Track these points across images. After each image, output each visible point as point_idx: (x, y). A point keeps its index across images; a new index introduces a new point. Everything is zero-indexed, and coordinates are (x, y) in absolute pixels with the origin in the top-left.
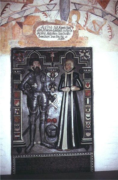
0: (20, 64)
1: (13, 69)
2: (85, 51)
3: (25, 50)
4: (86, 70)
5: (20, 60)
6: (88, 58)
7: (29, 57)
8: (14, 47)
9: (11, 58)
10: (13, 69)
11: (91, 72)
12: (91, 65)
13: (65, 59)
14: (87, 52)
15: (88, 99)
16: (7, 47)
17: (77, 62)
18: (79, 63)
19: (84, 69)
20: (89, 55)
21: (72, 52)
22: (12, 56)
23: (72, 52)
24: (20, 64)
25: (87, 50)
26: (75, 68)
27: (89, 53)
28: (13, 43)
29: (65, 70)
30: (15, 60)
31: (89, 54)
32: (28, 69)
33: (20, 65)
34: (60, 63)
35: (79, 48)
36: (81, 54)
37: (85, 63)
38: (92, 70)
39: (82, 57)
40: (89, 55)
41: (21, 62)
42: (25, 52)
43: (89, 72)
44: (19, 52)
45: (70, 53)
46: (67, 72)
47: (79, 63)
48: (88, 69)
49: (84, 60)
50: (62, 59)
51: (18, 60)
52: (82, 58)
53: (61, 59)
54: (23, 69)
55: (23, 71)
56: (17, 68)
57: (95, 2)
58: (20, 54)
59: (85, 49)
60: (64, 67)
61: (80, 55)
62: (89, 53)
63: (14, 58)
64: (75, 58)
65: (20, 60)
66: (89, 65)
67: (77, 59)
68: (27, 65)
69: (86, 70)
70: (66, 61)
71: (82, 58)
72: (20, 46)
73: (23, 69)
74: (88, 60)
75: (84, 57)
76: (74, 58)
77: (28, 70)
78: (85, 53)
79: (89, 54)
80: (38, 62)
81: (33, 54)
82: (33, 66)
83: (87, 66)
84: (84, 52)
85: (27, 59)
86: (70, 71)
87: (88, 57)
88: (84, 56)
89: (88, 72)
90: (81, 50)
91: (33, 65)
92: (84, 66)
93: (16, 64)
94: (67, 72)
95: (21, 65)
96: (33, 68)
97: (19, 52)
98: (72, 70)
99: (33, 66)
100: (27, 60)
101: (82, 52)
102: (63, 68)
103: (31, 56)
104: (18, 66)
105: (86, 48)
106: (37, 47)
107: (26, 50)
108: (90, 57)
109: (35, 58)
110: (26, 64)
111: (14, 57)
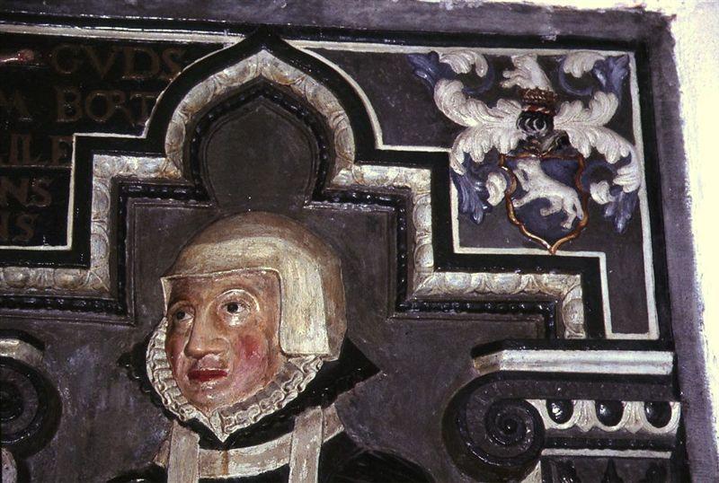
2: (529, 73)
4: (634, 414)
6: (599, 194)
11: (679, 444)
12: (664, 324)
13: (156, 189)
14: (583, 89)
15: (177, 191)
17: (404, 268)
18: (432, 280)
19: (564, 388)
20: (613, 148)
25: (579, 63)
26: (370, 370)
27: (606, 106)
29: (170, 397)
31: (619, 125)
34: (79, 257)
35: (442, 25)
36: (471, 116)
37: (550, 280)
38: (698, 406)
39: (494, 162)
40: (613, 148)
43: (642, 441)
45: (261, 88)
46: (208, 440)
47: (432, 280)
48: (610, 390)
49: (538, 219)
50: (122, 188)
52: (497, 188)
53: (100, 187)
57: (337, 117)
59: (530, 41)
60: (156, 353)
61: (451, 131)
62: (606, 106)
64: (358, 194)
66: (631, 316)
67: (400, 199)
69: (584, 414)
70: (204, 226)
71: (497, 188)
74: (596, 226)
75: (531, 168)
76: (345, 195)
78: (538, 111)
79: (619, 125)
83: (595, 340)
84: (516, 94)
86: (253, 415)
87: (599, 168)
88: (523, 148)
89: (623, 441)
90: (462, 59)
92: (533, 324)
94: (208, 440)
98: (316, 394)
101: (486, 90)
102: (136, 359)
105: (562, 15)
108: (632, 178)
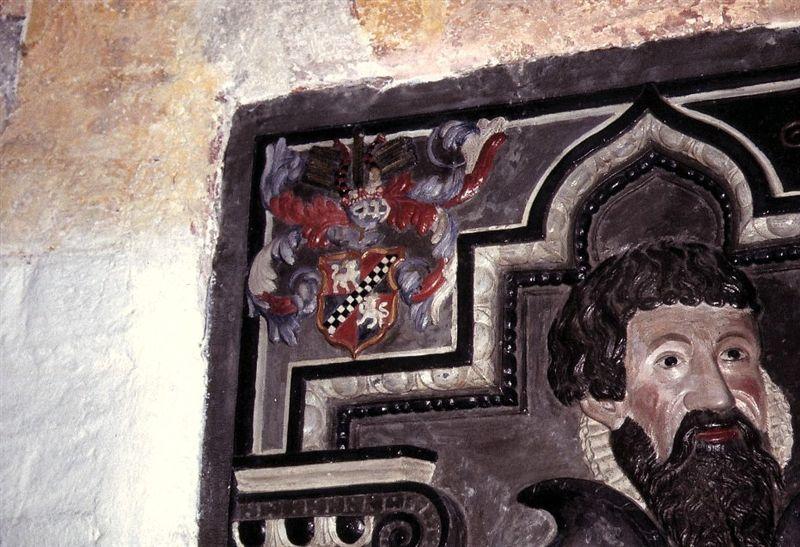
0: (376, 386)
1: (249, 481)
3: (470, 118)
5: (373, 311)
7: (535, 231)
8: (273, 87)
9: (217, 292)
10: (249, 481)
16: (162, 93)
21: (699, 149)
22: (240, 246)
23: (699, 149)
24: (376, 386)
28: (251, 77)
30: (280, 309)
32: (527, 481)
33: (372, 408)
41: (392, 335)
42: (473, 146)
44: (365, 159)
51: (331, 302)
54: (426, 473)
55: (423, 509)
56: (315, 457)
58: (371, 207)
63: (263, 279)
65: (373, 311)
68: (507, 394)
72: (381, 51)
73: (426, 473)
77: (530, 498)
80: (722, 314)
81: (629, 172)
82: (620, 413)
85: (514, 278)
91: (612, 383)
93: (302, 376)
95: (398, 404)
96: (627, 443)
97: (365, 159)
99: (620, 413)
100: (508, 313)
103: (581, 217)
104: (342, 416)
106: (703, 38)
107: (491, 112)
109: (669, 253)
110: (481, 370)
111: (263, 259)
